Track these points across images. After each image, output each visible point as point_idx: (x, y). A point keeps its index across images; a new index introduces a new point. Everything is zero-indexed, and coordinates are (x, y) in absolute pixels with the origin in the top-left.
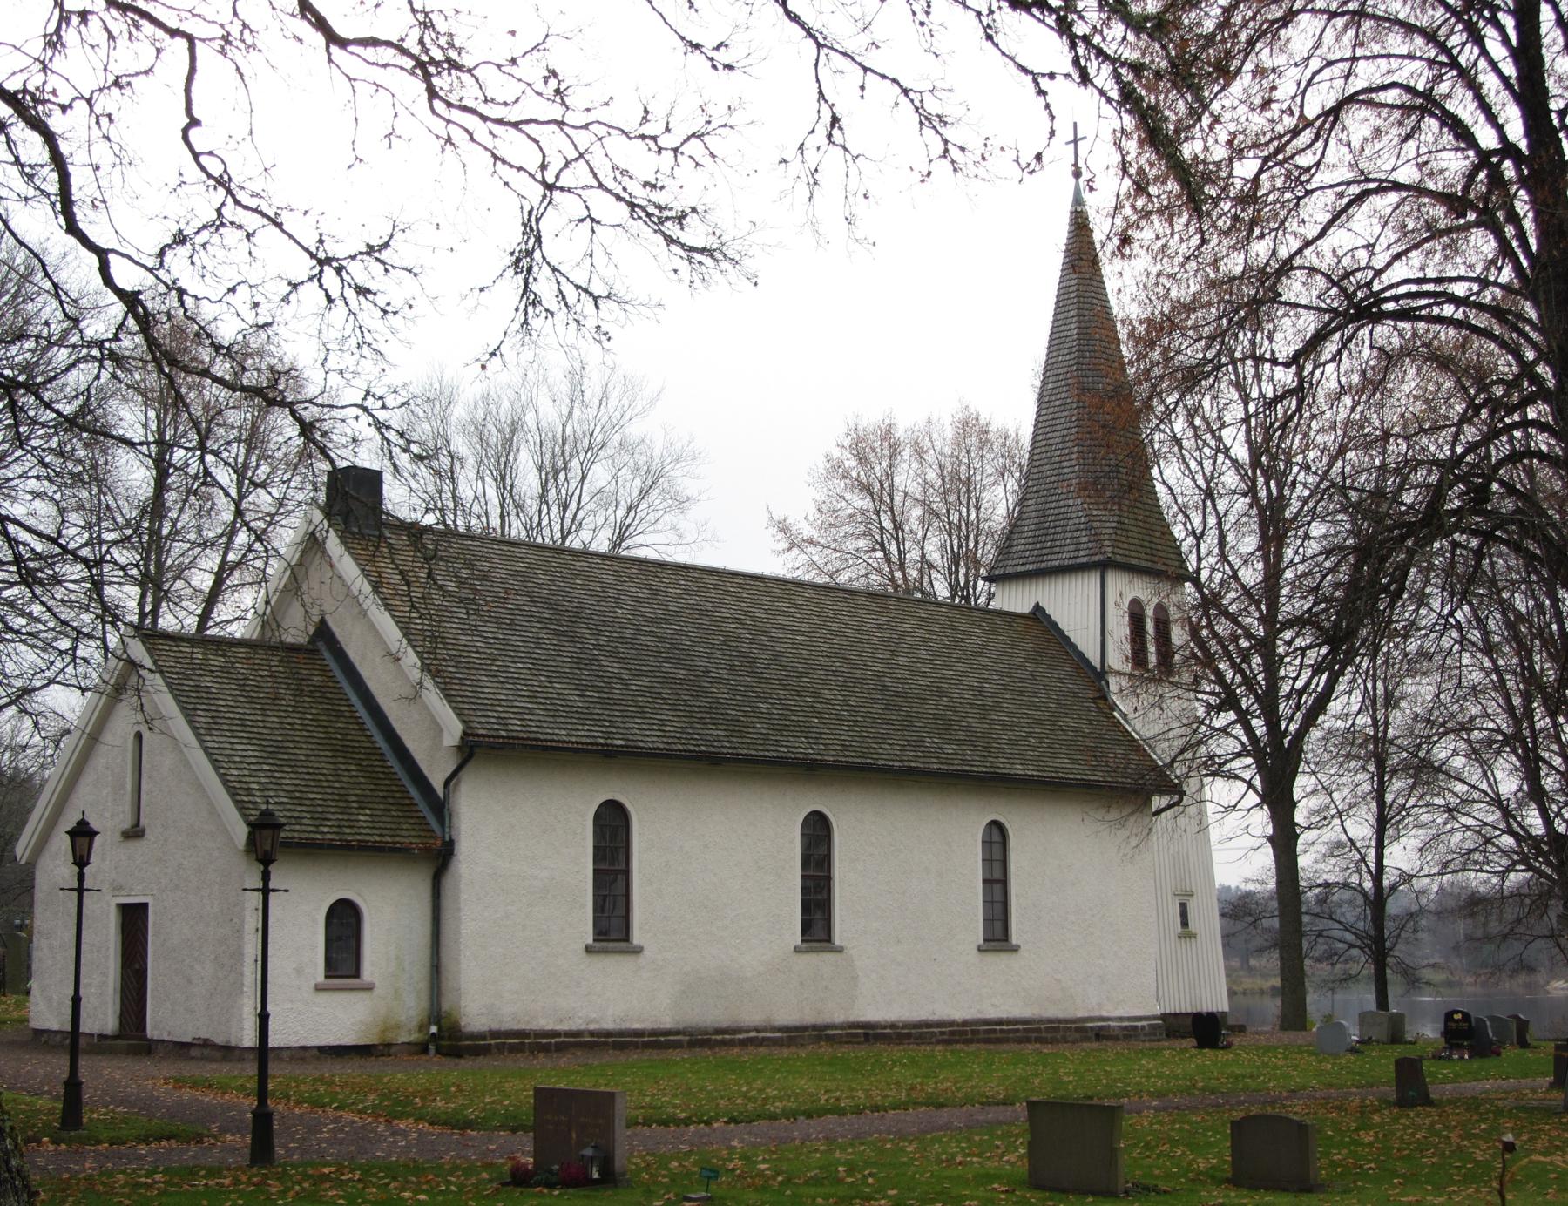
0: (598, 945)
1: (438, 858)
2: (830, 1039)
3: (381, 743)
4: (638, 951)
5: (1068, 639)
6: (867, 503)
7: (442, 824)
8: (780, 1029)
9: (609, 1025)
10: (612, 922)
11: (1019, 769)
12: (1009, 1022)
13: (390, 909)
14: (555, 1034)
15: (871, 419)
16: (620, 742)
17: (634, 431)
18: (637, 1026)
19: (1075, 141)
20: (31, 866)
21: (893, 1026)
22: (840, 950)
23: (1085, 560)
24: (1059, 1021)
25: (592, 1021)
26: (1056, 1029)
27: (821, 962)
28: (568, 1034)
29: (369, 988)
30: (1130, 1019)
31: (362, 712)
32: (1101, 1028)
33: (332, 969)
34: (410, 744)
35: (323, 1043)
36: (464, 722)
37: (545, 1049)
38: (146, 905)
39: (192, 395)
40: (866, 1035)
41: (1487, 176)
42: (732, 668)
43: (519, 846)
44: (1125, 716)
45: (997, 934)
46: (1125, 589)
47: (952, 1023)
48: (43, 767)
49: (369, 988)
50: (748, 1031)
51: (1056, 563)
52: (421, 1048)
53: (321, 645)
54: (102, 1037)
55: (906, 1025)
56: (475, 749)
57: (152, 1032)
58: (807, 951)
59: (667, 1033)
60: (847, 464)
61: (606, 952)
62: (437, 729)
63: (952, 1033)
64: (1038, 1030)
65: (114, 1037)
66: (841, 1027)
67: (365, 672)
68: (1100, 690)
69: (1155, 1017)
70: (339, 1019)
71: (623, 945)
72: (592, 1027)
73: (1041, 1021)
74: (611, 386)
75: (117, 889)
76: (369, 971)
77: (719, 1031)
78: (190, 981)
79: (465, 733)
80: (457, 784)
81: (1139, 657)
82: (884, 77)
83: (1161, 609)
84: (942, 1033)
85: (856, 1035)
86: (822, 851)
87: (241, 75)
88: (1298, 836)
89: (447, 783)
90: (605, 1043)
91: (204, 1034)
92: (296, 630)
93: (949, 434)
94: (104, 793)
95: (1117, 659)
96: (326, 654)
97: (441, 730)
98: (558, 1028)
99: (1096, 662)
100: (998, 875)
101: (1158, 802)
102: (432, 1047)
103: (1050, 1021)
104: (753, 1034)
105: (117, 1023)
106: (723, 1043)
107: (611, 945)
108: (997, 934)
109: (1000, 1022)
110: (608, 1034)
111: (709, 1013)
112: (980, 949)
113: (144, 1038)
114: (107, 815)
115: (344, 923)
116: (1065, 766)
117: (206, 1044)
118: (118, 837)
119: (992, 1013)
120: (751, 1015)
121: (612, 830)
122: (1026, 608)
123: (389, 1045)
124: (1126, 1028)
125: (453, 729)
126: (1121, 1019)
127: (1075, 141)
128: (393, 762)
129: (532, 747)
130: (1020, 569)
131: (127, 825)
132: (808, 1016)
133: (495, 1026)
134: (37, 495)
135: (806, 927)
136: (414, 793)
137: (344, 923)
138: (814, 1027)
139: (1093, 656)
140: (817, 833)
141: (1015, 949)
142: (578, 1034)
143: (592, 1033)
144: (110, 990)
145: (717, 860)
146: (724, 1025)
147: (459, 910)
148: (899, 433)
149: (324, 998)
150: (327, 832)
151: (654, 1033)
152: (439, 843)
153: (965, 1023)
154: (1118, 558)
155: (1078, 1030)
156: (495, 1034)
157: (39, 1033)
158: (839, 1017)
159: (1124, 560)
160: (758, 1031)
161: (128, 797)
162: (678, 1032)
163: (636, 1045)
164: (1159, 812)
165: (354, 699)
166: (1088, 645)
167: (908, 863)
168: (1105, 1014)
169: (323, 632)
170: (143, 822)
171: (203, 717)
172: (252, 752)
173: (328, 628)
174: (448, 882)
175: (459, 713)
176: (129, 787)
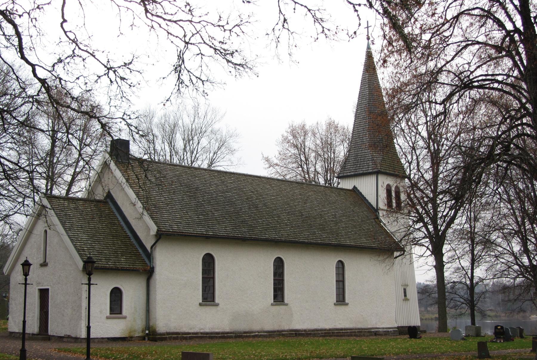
0: (204, 303)
1: (148, 273)
2: (283, 335)
3: (129, 234)
4: (217, 305)
5: (365, 198)
6: (296, 151)
7: (150, 262)
8: (266, 332)
9: (207, 330)
10: (208, 295)
11: (348, 242)
12: (345, 329)
13: (132, 291)
14: (189, 333)
15: (297, 122)
16: (211, 233)
17: (216, 126)
18: (217, 331)
19: (368, 27)
20: (8, 276)
21: (305, 331)
22: (287, 305)
23: (371, 171)
24: (362, 329)
25: (202, 329)
26: (361, 332)
27: (280, 309)
28: (193, 333)
29: (125, 318)
30: (386, 328)
31: (123, 223)
32: (376, 331)
33: (112, 311)
34: (139, 234)
35: (109, 337)
36: (158, 226)
37: (186, 339)
38: (48, 289)
39: (64, 114)
40: (296, 334)
41: (509, 39)
42: (249, 208)
43: (177, 269)
44: (385, 224)
45: (341, 299)
46: (385, 181)
47: (325, 330)
48: (13, 242)
49: (125, 318)
50: (255, 332)
51: (361, 172)
52: (143, 338)
53: (108, 200)
54: (33, 334)
55: (310, 330)
56: (160, 236)
57: (50, 333)
58: (276, 305)
59: (228, 333)
60: (289, 138)
61: (206, 305)
62: (148, 229)
63: (325, 333)
64: (355, 332)
65: (37, 335)
66: (287, 331)
67: (123, 209)
68: (376, 215)
69: (395, 328)
70: (114, 328)
71: (212, 303)
72: (202, 331)
73: (356, 329)
74: (208, 111)
75: (38, 284)
76: (125, 312)
77: (245, 332)
78: (63, 315)
79: (158, 230)
80: (155, 248)
81: (389, 204)
82: (302, 5)
83: (397, 188)
84: (322, 333)
85: (292, 334)
86: (281, 271)
87: (81, 5)
88: (444, 266)
89: (152, 247)
90: (206, 337)
91: (68, 334)
92: (100, 195)
93: (324, 128)
94: (34, 251)
95: (382, 205)
96: (110, 203)
97: (150, 229)
98: (190, 331)
99: (374, 205)
100: (341, 279)
101: (396, 254)
102: (146, 338)
103: (359, 329)
104: (257, 333)
105: (38, 329)
106: (247, 337)
107: (208, 303)
108: (341, 299)
109: (342, 329)
110: (207, 333)
111: (242, 326)
112: (335, 304)
113: (48, 335)
114: (35, 258)
115: (116, 296)
116: (364, 241)
117: (69, 337)
118: (39, 266)
119: (339, 326)
120: (256, 327)
121: (209, 263)
122: (350, 187)
123: (132, 337)
124: (385, 331)
125: (154, 229)
126: (383, 328)
127: (368, 27)
128: (133, 240)
129: (181, 235)
130: (349, 174)
131: (42, 262)
132: (276, 328)
133: (168, 331)
134: (11, 149)
135: (275, 297)
136: (140, 251)
137: (116, 296)
138: (278, 331)
139: (374, 204)
140: (279, 264)
141: (347, 304)
142: (197, 333)
143: (202, 333)
144: (36, 318)
145: (244, 274)
146: (247, 330)
147: (156, 291)
148: (307, 127)
149: (110, 321)
150: (110, 264)
151: (223, 333)
152: (149, 268)
153: (330, 330)
154: (382, 170)
155: (368, 332)
156: (168, 334)
157: (11, 333)
158: (286, 328)
159: (384, 171)
160: (259, 332)
161: (42, 252)
162: (231, 333)
163: (217, 337)
164: (396, 257)
165: (120, 219)
166: (372, 200)
167: (310, 274)
168: (378, 327)
169: (109, 196)
170: (47, 261)
171: (68, 225)
172: (85, 237)
173: (111, 194)
174: (152, 281)
175: (156, 223)
176: (42, 249)
